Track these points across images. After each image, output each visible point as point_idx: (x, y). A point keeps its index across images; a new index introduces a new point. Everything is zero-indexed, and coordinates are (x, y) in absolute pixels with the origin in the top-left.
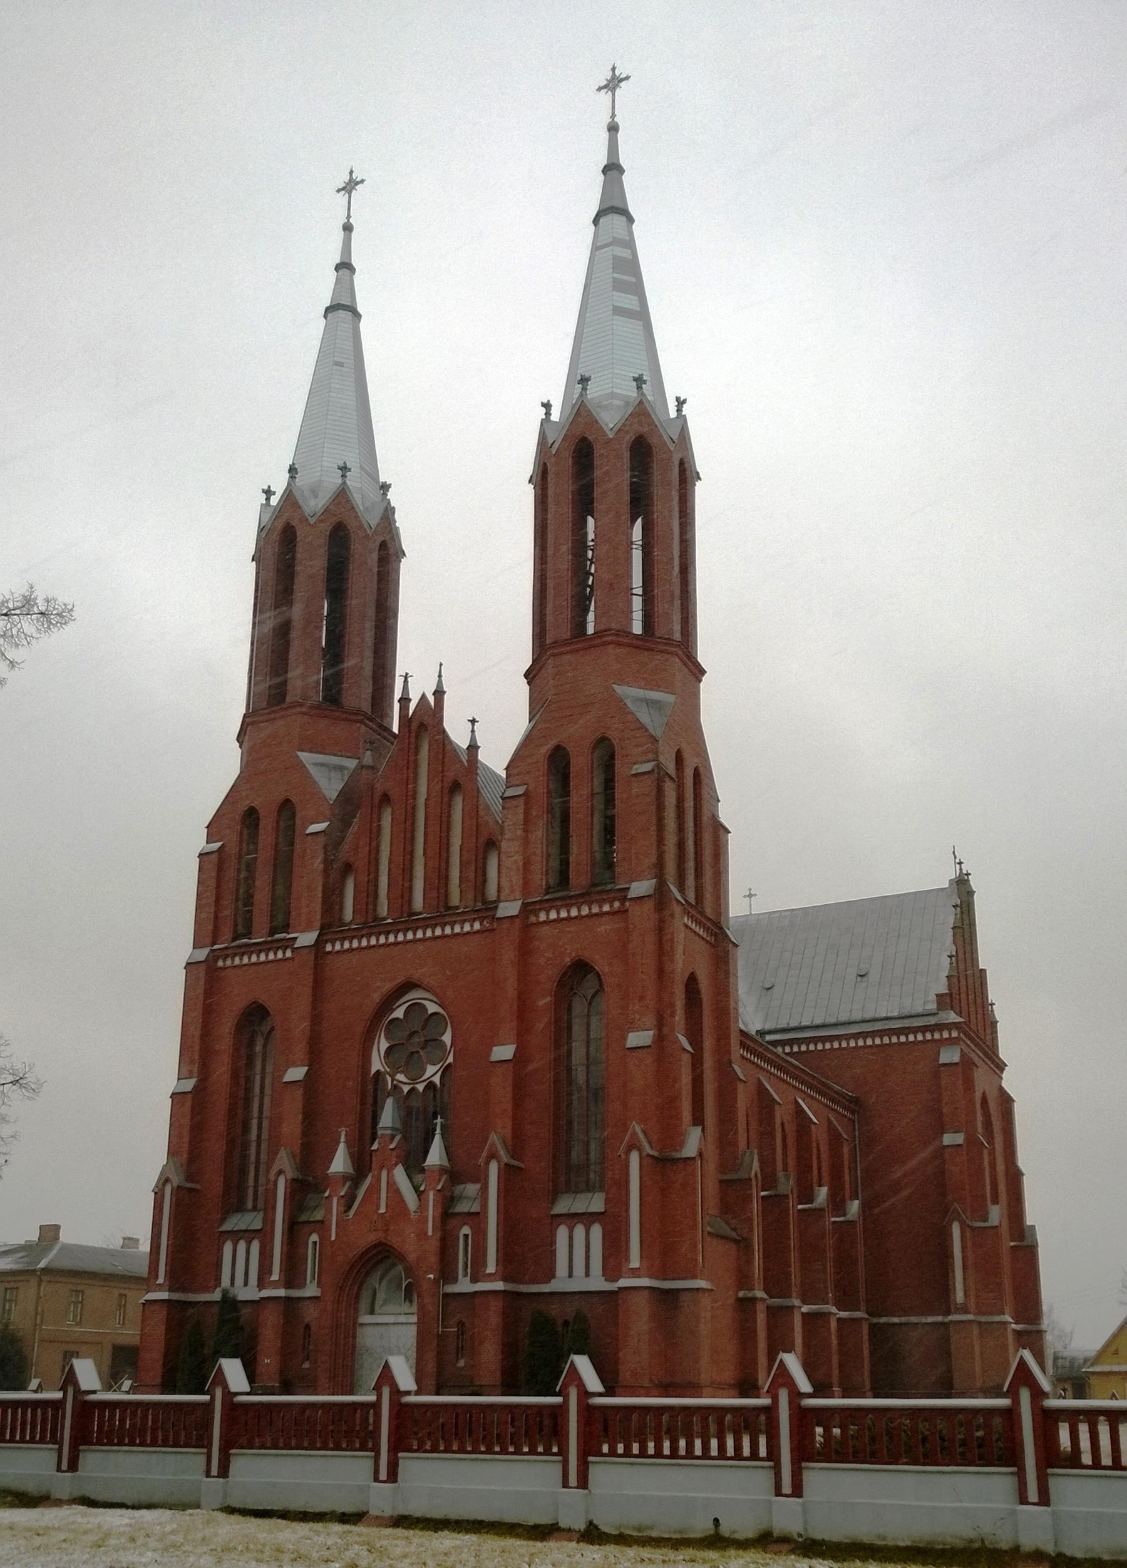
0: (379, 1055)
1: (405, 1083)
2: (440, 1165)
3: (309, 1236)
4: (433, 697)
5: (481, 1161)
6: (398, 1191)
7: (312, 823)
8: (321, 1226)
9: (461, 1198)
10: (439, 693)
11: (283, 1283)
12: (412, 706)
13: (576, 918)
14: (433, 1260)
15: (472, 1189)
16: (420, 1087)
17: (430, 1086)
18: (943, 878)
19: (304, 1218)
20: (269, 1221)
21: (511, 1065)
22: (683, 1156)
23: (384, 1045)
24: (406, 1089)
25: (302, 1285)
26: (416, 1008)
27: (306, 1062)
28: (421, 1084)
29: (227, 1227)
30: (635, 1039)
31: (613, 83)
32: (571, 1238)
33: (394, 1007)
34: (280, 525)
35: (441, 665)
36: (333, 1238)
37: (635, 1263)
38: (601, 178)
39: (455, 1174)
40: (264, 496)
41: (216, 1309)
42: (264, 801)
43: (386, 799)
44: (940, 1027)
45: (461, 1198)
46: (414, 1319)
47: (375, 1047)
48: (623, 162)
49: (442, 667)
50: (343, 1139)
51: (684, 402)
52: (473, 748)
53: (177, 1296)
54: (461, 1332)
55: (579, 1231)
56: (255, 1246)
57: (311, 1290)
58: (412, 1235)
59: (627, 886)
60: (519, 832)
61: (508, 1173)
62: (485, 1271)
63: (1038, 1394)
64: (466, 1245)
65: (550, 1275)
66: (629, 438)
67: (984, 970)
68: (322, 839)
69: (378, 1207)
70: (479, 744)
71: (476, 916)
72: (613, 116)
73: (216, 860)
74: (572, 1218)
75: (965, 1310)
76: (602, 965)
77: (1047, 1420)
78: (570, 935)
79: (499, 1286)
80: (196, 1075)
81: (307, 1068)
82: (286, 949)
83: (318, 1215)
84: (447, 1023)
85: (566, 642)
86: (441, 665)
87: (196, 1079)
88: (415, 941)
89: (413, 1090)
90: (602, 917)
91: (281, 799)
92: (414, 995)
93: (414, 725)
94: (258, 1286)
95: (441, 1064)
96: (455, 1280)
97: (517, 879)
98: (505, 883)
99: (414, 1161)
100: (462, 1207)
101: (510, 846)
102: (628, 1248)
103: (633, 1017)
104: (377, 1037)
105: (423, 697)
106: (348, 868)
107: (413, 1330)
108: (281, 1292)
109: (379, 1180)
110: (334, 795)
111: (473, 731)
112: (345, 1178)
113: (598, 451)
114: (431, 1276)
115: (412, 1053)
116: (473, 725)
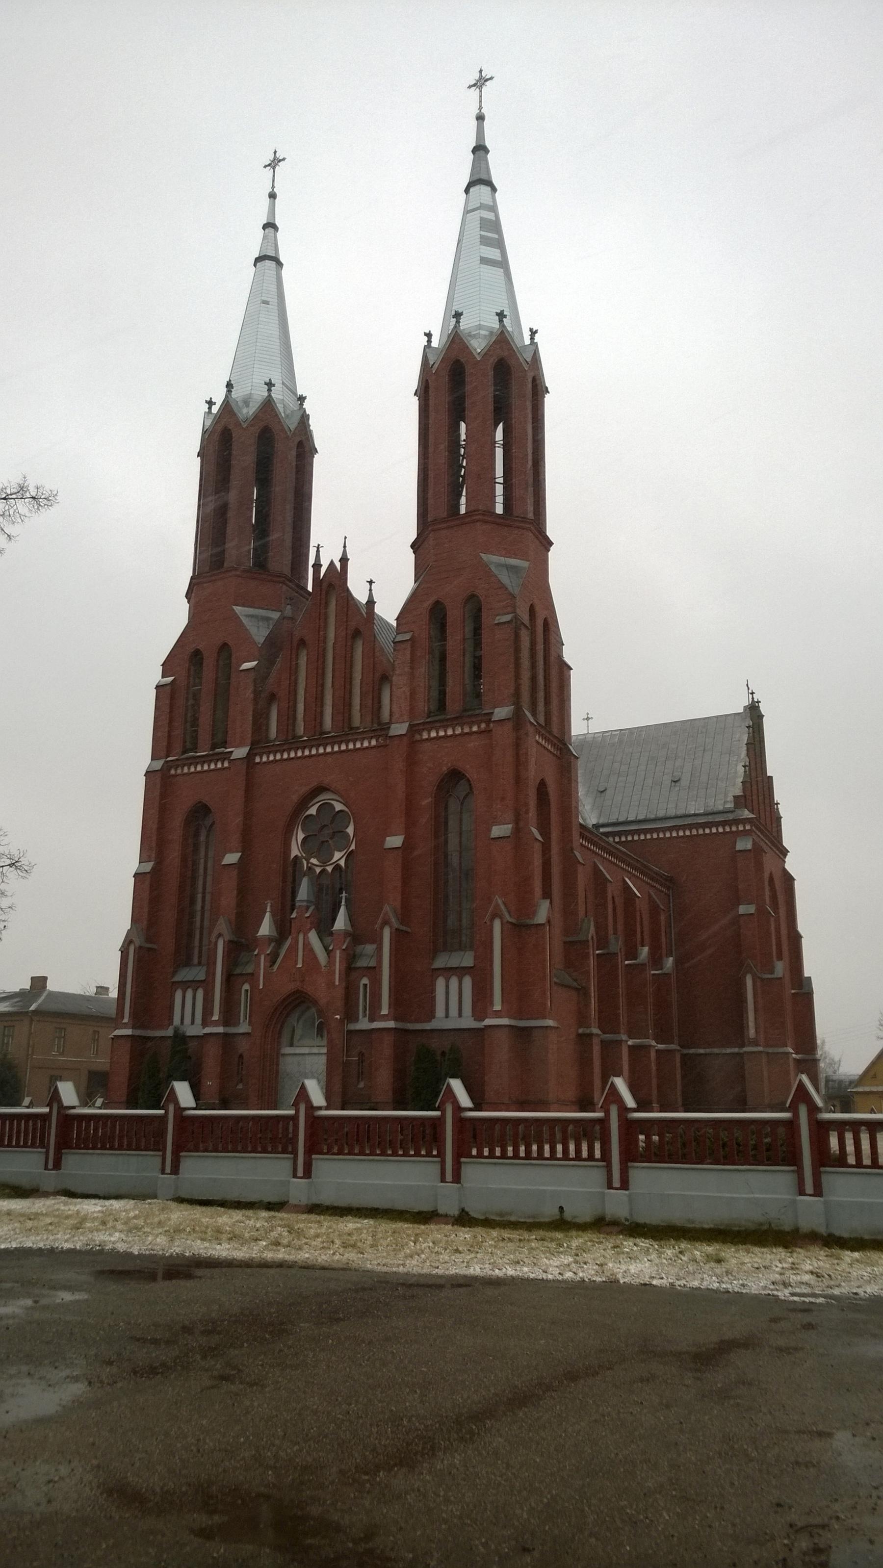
1: (317, 866)
4: (339, 563)
5: (377, 926)
6: (312, 950)
8: (252, 977)
10: (344, 560)
12: (323, 570)
13: (451, 736)
14: (340, 1004)
15: (370, 948)
16: (329, 869)
18: (738, 705)
20: (211, 974)
23: (301, 836)
24: (318, 870)
25: (237, 1024)
26: (326, 807)
29: (177, 978)
30: (497, 831)
31: (481, 82)
32: (447, 987)
35: (346, 538)
36: (261, 987)
37: (497, 1007)
38: (472, 156)
40: (207, 406)
43: (302, 643)
44: (736, 822)
46: (324, 1050)
47: (294, 837)
51: (536, 332)
52: (371, 603)
53: (138, 1032)
55: (454, 982)
56: (200, 993)
57: (244, 1028)
60: (406, 669)
61: (399, 936)
63: (813, 1109)
66: (493, 360)
67: (771, 777)
75: (756, 1043)
76: (471, 773)
77: (821, 1129)
79: (391, 1024)
80: (153, 859)
81: (240, 854)
82: (224, 761)
86: (346, 538)
87: (153, 863)
88: (325, 754)
89: (323, 871)
92: (324, 797)
93: (325, 585)
94: (202, 1025)
96: (356, 1020)
99: (324, 927)
100: (362, 963)
105: (332, 563)
106: (272, 697)
107: (324, 1059)
108: (220, 1030)
110: (262, 640)
111: (370, 590)
112: (270, 939)
113: (469, 370)
114: (338, 1017)
115: (323, 842)
116: (371, 585)
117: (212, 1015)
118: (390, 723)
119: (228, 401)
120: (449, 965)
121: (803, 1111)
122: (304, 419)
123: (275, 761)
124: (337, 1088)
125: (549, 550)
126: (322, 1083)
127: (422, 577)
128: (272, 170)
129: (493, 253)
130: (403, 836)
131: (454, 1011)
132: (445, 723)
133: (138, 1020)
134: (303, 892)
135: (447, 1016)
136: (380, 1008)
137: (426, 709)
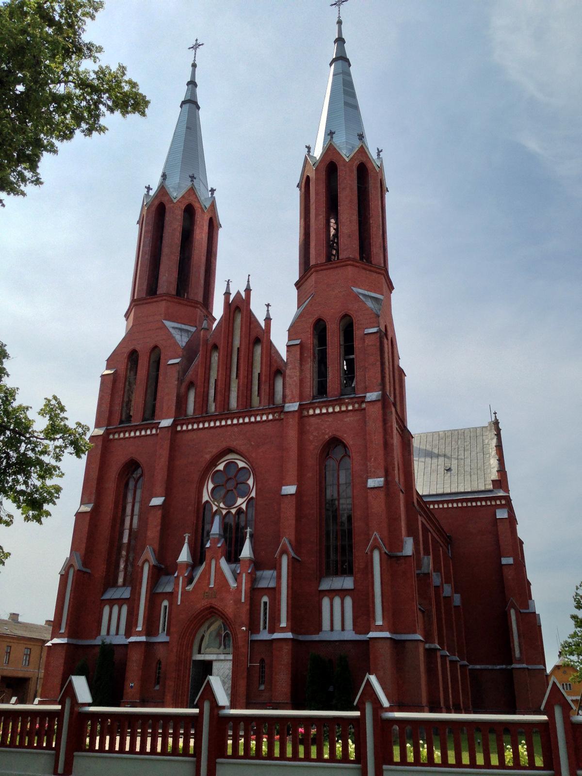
0: (208, 492)
2: (250, 557)
3: (162, 602)
4: (244, 293)
6: (222, 573)
7: (171, 359)
8: (171, 596)
9: (261, 578)
10: (248, 290)
11: (144, 632)
12: (232, 298)
13: (332, 413)
14: (244, 616)
16: (233, 511)
17: (240, 511)
18: (485, 420)
19: (160, 590)
20: (135, 593)
21: (294, 497)
22: (404, 555)
23: (211, 486)
24: (224, 512)
25: (156, 634)
27: (164, 495)
28: (234, 509)
29: (107, 596)
30: (372, 483)
31: (196, 46)
33: (217, 464)
34: (156, 203)
35: (249, 275)
36: (179, 603)
37: (379, 622)
39: (258, 564)
40: (146, 190)
41: (98, 650)
42: (143, 347)
43: (215, 347)
45: (261, 578)
46: (230, 657)
47: (205, 487)
48: (197, 81)
49: (250, 277)
50: (186, 541)
51: (381, 151)
53: (74, 641)
54: (262, 667)
56: (125, 609)
57: (162, 638)
58: (231, 602)
59: (364, 395)
61: (294, 563)
62: (280, 625)
64: (265, 609)
65: (319, 629)
66: (357, 163)
68: (178, 367)
69: (209, 584)
70: (271, 318)
71: (270, 411)
72: (195, 60)
73: (112, 378)
74: (112, 602)
75: (520, 661)
76: (349, 440)
78: (328, 423)
79: (289, 635)
80: (93, 502)
81: (164, 498)
82: (152, 429)
83: (169, 589)
84: (250, 473)
85: (322, 265)
86: (249, 275)
87: (92, 505)
88: (233, 425)
89: (229, 513)
90: (348, 413)
91: (152, 345)
92: (230, 457)
93: (232, 309)
94: (125, 635)
95: (246, 498)
96: (258, 632)
97: (296, 392)
98: (288, 392)
99: (233, 556)
100: (263, 584)
101: (292, 374)
102: (374, 612)
103: (370, 469)
104: (206, 482)
105: (238, 293)
106: (191, 384)
107: (229, 665)
108: (143, 639)
109: (210, 566)
110: (184, 344)
111: (268, 311)
112: (187, 565)
114: (244, 628)
115: (228, 491)
116: (268, 307)
117: (136, 627)
118: (284, 402)
119: (163, 186)
120: (333, 588)
121: (558, 712)
122: (213, 205)
123: (193, 430)
124: (242, 689)
125: (391, 293)
126: (227, 685)
127: (310, 298)
128: (194, 51)
129: (350, 100)
130: (296, 486)
131: (337, 626)
132: (327, 404)
133: (72, 632)
134: (216, 528)
135: (332, 629)
136: (279, 621)
137: (311, 393)
